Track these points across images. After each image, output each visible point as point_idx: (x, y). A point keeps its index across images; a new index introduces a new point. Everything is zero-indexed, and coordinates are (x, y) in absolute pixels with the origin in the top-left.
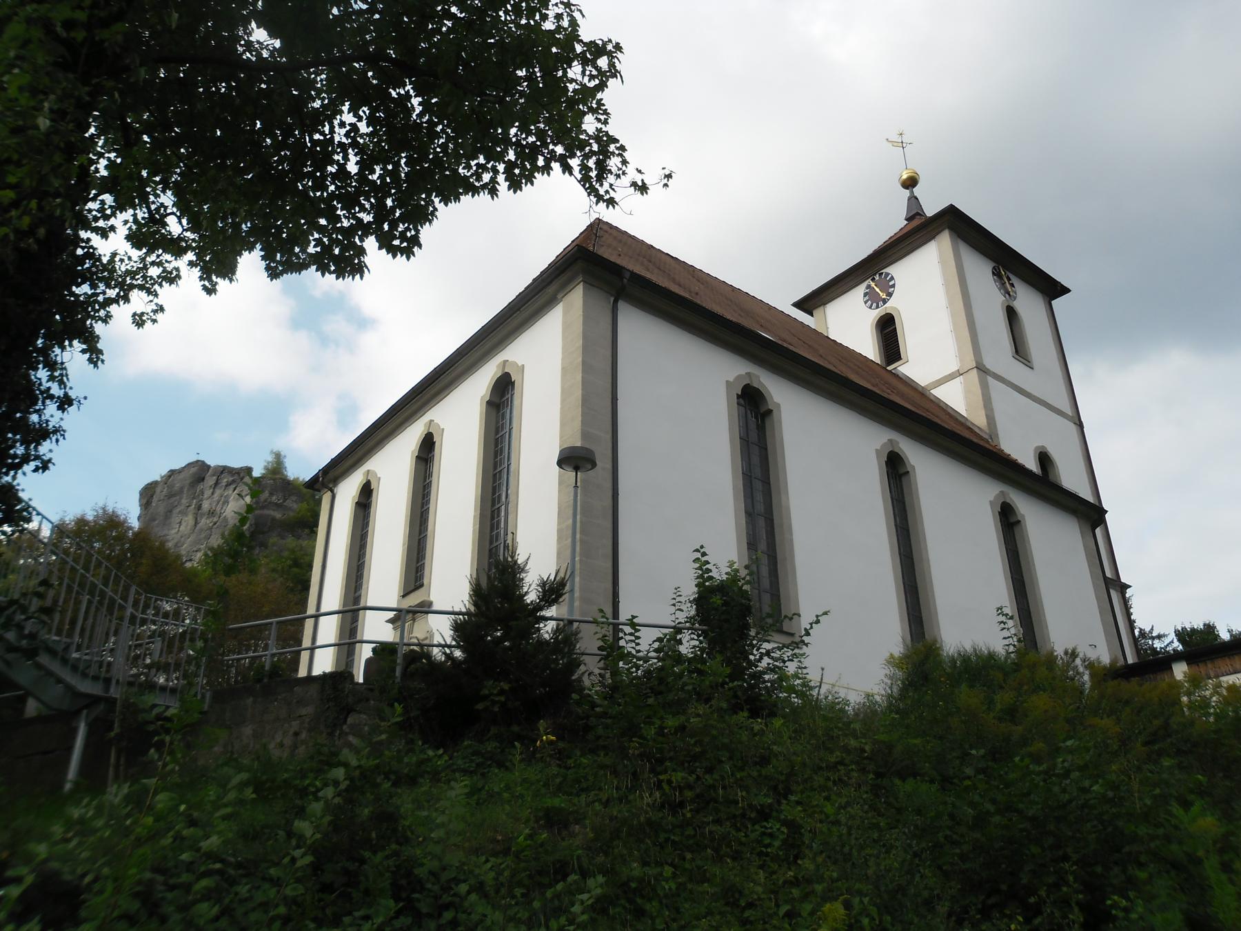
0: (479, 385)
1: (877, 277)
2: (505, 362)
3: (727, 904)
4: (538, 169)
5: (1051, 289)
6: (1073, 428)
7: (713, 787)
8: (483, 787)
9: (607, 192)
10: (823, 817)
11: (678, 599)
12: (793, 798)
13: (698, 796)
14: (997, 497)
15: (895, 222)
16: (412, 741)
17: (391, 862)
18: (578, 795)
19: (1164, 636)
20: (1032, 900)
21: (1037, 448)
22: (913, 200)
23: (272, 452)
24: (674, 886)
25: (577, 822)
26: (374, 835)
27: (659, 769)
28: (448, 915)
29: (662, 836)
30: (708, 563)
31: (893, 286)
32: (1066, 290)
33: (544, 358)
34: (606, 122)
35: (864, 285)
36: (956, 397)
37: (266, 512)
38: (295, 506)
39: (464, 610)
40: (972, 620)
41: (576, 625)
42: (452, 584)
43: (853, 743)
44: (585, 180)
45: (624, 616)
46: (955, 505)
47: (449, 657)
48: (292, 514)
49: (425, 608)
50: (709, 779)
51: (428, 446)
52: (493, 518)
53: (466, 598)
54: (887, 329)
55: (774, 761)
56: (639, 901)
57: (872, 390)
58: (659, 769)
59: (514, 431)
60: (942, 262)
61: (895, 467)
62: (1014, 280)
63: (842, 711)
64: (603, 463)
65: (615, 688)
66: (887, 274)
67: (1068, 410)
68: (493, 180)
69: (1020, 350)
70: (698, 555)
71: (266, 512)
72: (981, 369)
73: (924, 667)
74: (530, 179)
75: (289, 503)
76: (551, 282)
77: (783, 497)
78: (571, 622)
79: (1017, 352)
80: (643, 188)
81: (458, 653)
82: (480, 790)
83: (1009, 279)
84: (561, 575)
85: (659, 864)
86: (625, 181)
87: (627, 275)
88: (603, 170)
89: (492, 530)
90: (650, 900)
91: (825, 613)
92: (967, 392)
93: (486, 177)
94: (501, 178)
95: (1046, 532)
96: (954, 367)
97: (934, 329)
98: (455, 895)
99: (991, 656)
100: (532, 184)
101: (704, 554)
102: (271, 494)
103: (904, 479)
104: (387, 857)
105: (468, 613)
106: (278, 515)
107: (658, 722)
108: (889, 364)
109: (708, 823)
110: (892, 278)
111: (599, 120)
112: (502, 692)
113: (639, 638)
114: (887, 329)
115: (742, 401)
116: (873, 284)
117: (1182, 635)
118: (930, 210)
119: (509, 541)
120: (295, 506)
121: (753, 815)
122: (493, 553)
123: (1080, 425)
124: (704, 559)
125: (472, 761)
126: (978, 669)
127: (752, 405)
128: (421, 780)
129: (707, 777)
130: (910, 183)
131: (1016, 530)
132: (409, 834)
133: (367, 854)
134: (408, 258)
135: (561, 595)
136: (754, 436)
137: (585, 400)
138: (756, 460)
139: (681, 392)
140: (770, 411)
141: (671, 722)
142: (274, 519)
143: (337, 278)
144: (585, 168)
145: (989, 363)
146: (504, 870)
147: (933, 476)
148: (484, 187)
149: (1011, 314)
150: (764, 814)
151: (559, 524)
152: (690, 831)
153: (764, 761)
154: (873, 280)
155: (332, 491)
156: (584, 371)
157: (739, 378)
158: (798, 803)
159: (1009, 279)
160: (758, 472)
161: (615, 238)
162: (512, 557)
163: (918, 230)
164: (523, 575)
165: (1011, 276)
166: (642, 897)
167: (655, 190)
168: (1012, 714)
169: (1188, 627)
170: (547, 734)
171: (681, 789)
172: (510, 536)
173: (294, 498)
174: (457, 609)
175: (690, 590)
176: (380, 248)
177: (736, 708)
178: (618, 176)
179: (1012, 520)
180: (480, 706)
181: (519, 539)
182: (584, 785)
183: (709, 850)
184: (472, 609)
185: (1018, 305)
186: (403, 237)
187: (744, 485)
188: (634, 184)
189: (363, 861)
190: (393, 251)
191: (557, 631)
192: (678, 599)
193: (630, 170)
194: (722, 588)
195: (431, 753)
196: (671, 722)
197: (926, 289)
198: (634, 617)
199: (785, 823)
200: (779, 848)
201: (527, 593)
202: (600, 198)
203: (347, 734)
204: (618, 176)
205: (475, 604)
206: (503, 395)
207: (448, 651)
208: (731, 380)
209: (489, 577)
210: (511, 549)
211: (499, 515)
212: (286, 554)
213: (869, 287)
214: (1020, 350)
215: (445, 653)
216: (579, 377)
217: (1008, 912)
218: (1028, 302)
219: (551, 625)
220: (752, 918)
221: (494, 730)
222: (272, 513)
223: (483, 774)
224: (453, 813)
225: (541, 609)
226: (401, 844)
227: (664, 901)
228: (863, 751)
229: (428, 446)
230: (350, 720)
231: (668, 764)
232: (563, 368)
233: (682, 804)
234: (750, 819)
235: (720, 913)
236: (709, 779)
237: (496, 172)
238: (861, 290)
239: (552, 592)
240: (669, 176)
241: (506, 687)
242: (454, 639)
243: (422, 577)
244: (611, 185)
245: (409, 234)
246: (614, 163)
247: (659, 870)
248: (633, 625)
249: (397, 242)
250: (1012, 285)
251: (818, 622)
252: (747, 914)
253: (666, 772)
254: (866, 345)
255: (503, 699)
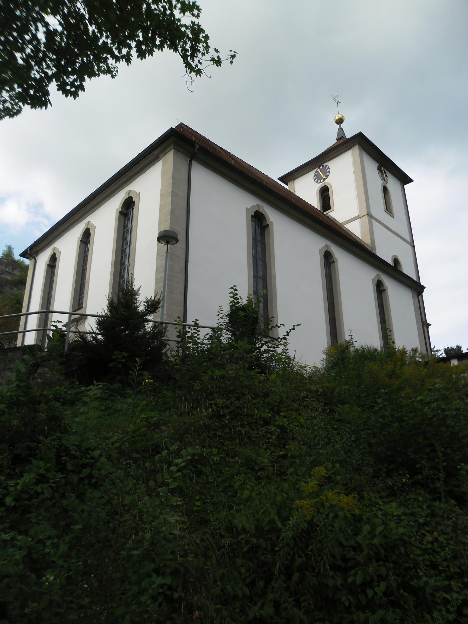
0: (114, 204)
1: (321, 167)
2: (130, 191)
3: (248, 468)
4: (156, 46)
5: (405, 179)
6: (410, 248)
7: (239, 407)
8: (112, 406)
9: (196, 66)
10: (299, 424)
11: (221, 312)
12: (282, 414)
13: (231, 412)
14: (375, 277)
15: (332, 141)
16: (73, 382)
17: (55, 442)
18: (164, 411)
19: (439, 350)
20: (418, 466)
21: (393, 256)
22: (341, 130)
23: (7, 246)
24: (218, 459)
25: (164, 424)
26: (46, 428)
27: (210, 398)
28: (86, 472)
29: (212, 433)
30: (237, 294)
31: (329, 172)
32: (410, 181)
33: (151, 189)
34: (198, 16)
35: (314, 171)
36: (356, 229)
37: (3, 276)
38: (18, 274)
39: (104, 314)
40: (362, 332)
41: (164, 325)
42: (98, 302)
43: (313, 388)
44: (184, 57)
45: (190, 321)
46: (355, 279)
47: (95, 339)
48: (16, 277)
49: (84, 317)
50: (237, 403)
51: (87, 236)
52: (120, 273)
53: (106, 308)
54: (325, 194)
55: (272, 396)
56: (199, 466)
57: (317, 220)
58: (210, 398)
59: (133, 228)
60: (354, 161)
61: (328, 258)
62: (388, 173)
63: (302, 375)
64: (182, 238)
65: (185, 357)
66: (326, 166)
67: (408, 239)
68: (129, 54)
69: (388, 208)
70: (232, 290)
71: (3, 276)
72: (369, 215)
73: (341, 354)
74: (151, 53)
75: (15, 272)
76: (156, 148)
77: (273, 269)
78: (162, 323)
79: (387, 209)
80: (218, 62)
81: (100, 337)
82: (110, 408)
83: (385, 173)
84: (158, 297)
85: (210, 447)
86: (208, 57)
87: (197, 147)
88: (195, 50)
89: (120, 279)
90: (205, 466)
91: (298, 325)
92: (362, 226)
93: (125, 51)
94: (134, 52)
95: (397, 295)
96: (356, 214)
97: (348, 193)
98: (92, 458)
99: (376, 350)
100: (152, 55)
101: (235, 290)
102: (6, 267)
103: (332, 265)
104: (54, 440)
105: (106, 316)
106: (9, 278)
107: (210, 373)
108: (324, 211)
109: (238, 426)
110: (329, 168)
111: (193, 15)
112: (124, 357)
113: (199, 331)
114: (325, 194)
115: (254, 219)
116: (319, 170)
117: (447, 351)
118: (349, 135)
119: (130, 278)
120: (18, 274)
121: (261, 422)
122: (120, 284)
123: (414, 247)
124: (236, 292)
125: (106, 393)
126: (366, 355)
127: (258, 220)
128: (77, 403)
129: (237, 402)
130: (340, 121)
131: (383, 294)
132: (68, 428)
133: (41, 438)
134: (75, 98)
135: (158, 308)
136: (259, 237)
137: (173, 212)
138: (259, 250)
139: (222, 211)
140: (268, 226)
141: (218, 373)
142: (7, 280)
143: (32, 108)
144: (184, 50)
145: (373, 213)
146: (125, 441)
147: (345, 263)
148: (123, 57)
149: (385, 190)
150: (267, 422)
151: (156, 275)
152: (227, 430)
153: (266, 395)
154: (319, 168)
155: (35, 259)
156: (172, 196)
157: (253, 207)
158: (284, 417)
159: (385, 173)
160: (260, 256)
161: (190, 133)
162: (131, 287)
163: (342, 145)
164: (137, 296)
165: (386, 171)
166: (201, 464)
167: (225, 63)
168: (392, 375)
169: (450, 347)
170: (148, 379)
171: (223, 408)
172: (130, 275)
173: (18, 270)
174: (100, 314)
175: (227, 309)
176: (58, 90)
177: (251, 368)
178: (203, 54)
179: (382, 289)
180: (111, 365)
181: (135, 277)
182: (168, 406)
183: (237, 440)
184: (109, 314)
185: (389, 186)
186: (72, 84)
187: (253, 262)
188: (213, 59)
189: (39, 442)
190: (66, 93)
191: (154, 327)
192: (221, 312)
193: (211, 50)
194: (243, 308)
195: (83, 389)
196: (218, 373)
197: (345, 173)
198: (197, 320)
199: (278, 426)
200: (275, 440)
201: (139, 306)
202: (192, 69)
203: (37, 378)
204: (203, 54)
205: (110, 311)
206: (128, 209)
207: (94, 335)
208: (249, 207)
209: (118, 297)
210: (131, 283)
211: (124, 271)
212: (13, 297)
213: (317, 172)
214: (388, 208)
215: (92, 337)
216: (170, 199)
217: (401, 472)
218: (393, 184)
219: (151, 324)
220: (262, 476)
221: (118, 378)
222: (6, 276)
223: (112, 400)
224: (94, 420)
225: (146, 315)
226: (62, 434)
227: (213, 467)
228: (318, 391)
229: (87, 236)
230: (39, 371)
231: (215, 395)
232: (161, 194)
233: (224, 416)
234: (260, 424)
235: (244, 473)
236: (237, 403)
237: (130, 47)
238: (313, 173)
239: (153, 306)
240: (233, 56)
241: (126, 355)
242: (97, 329)
243: (82, 303)
244: (199, 61)
245: (76, 84)
246: (201, 47)
247: (211, 450)
248: (196, 325)
249: (68, 88)
250: (386, 176)
251: (294, 329)
252: (259, 474)
253: (214, 399)
254: (314, 201)
255: (124, 361)
